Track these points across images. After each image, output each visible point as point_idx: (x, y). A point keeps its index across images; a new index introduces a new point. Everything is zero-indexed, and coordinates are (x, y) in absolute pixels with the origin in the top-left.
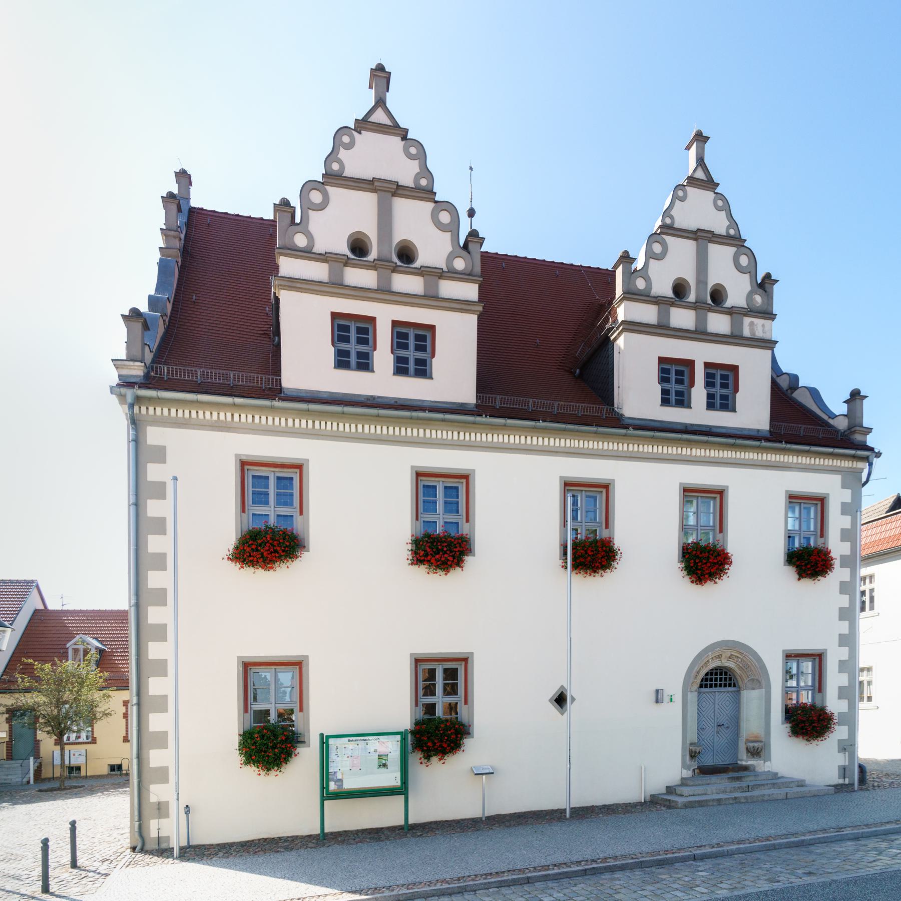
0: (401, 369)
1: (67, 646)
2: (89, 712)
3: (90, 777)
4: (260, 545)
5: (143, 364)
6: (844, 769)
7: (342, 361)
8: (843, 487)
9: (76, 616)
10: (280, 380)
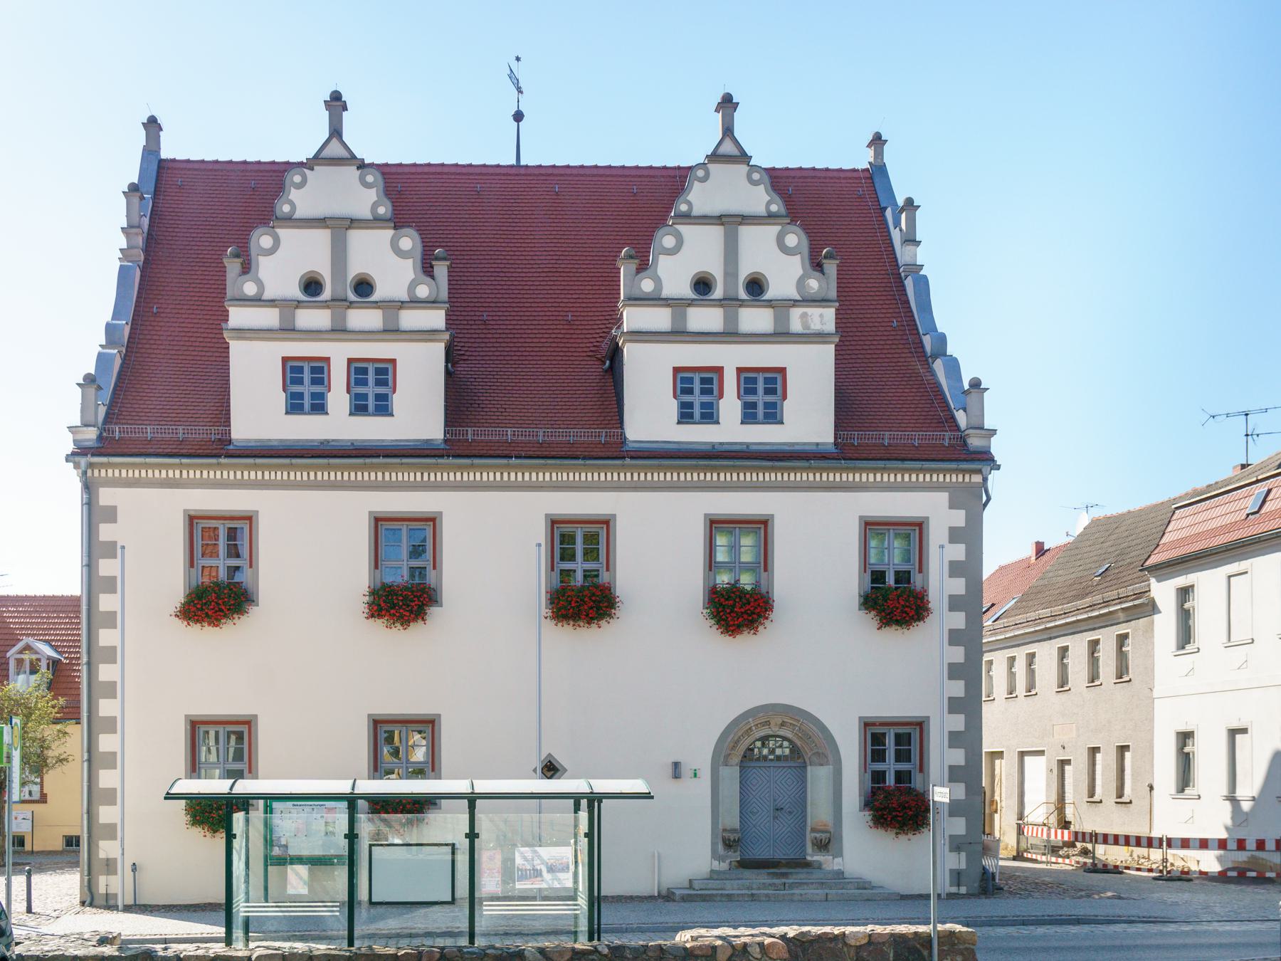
0: (359, 408)
1: (8, 655)
2: (39, 757)
3: (38, 852)
4: (205, 604)
5: (96, 429)
6: (959, 873)
7: (295, 406)
8: (951, 507)
9: (20, 606)
10: (230, 430)
